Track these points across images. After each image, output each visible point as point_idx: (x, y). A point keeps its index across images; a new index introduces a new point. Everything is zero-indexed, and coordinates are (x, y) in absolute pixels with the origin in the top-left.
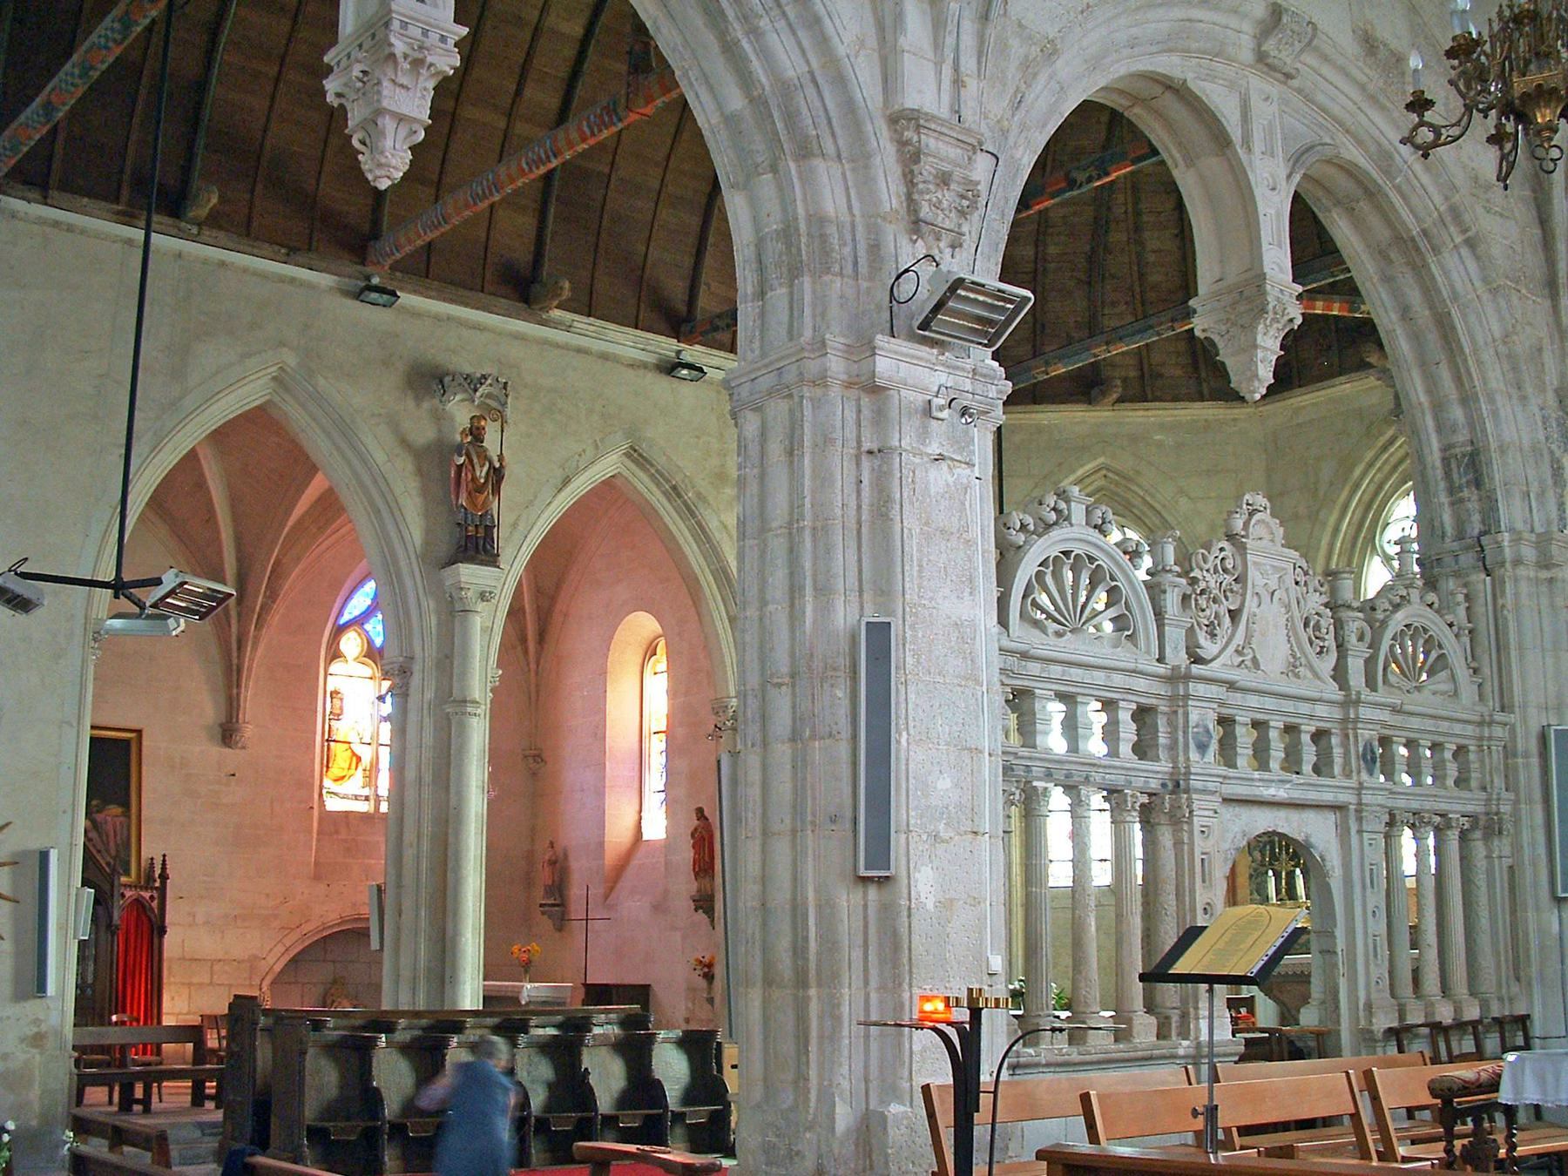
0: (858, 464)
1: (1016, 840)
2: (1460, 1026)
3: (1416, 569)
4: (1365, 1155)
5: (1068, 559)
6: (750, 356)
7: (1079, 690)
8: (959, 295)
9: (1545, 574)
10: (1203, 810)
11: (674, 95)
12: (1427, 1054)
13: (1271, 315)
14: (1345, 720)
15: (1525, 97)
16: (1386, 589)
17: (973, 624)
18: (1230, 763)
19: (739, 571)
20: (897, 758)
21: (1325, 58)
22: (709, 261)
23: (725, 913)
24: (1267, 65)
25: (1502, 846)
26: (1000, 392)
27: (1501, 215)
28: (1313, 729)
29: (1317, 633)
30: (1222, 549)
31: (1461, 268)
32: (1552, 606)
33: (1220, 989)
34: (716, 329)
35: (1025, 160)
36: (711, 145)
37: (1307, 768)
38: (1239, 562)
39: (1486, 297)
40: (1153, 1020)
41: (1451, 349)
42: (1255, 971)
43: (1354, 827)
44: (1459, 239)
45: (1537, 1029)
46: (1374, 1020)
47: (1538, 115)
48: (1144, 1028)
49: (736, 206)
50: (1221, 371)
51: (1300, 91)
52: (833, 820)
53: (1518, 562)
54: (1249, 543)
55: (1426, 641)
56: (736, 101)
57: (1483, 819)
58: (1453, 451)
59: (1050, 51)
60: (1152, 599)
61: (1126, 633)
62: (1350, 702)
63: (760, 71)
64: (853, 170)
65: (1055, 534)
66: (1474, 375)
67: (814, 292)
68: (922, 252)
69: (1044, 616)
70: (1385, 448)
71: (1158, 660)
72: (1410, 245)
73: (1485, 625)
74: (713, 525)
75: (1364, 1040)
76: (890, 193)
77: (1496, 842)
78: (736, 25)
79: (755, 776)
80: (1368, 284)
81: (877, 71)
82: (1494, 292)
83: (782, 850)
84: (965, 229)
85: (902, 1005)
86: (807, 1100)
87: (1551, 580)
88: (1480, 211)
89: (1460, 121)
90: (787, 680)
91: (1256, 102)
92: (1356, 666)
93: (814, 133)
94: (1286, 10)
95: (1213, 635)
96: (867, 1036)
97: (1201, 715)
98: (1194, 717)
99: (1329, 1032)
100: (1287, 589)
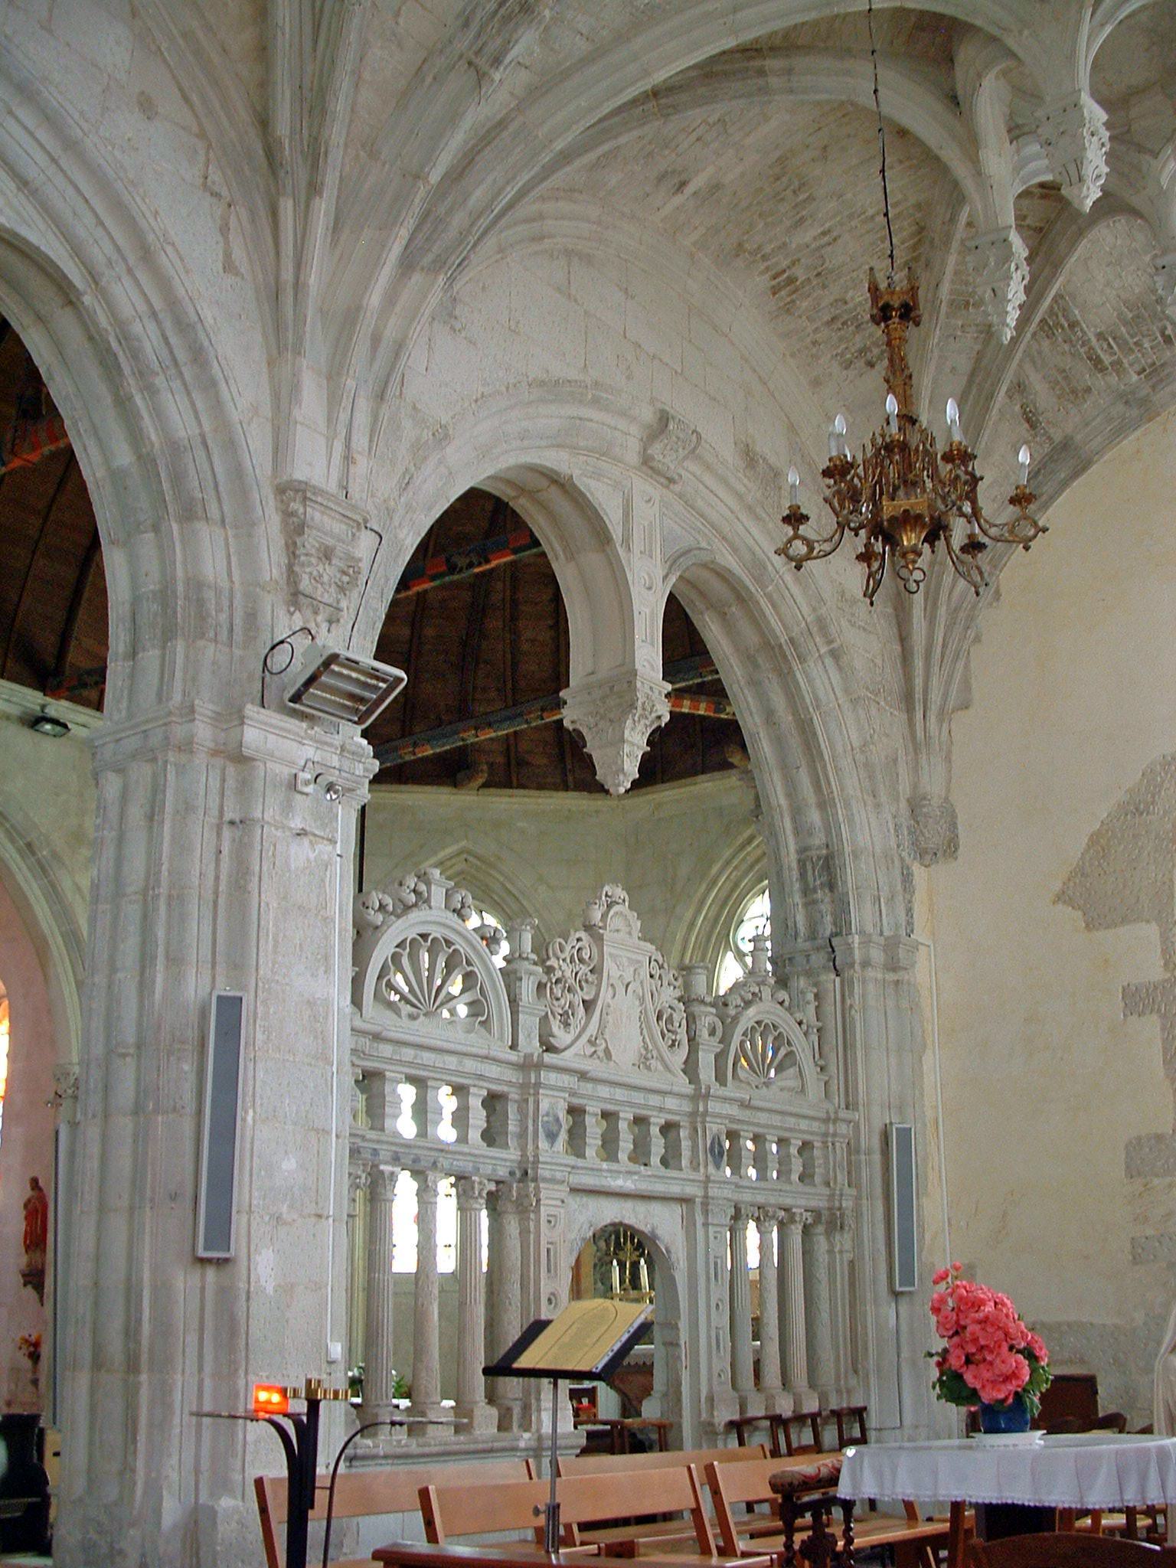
0: (219, 835)
1: (359, 1223)
2: (800, 1419)
3: (769, 967)
4: (706, 1551)
5: (426, 941)
6: (116, 717)
7: (432, 1075)
8: (333, 671)
9: (891, 977)
10: (550, 1199)
11: (62, 444)
12: (768, 1447)
13: (640, 711)
14: (694, 1114)
15: (893, 520)
16: (736, 987)
17: (327, 1002)
18: (581, 1155)
19: (90, 935)
20: (242, 1136)
21: (708, 467)
22: (82, 614)
23: (55, 1289)
24: (651, 468)
25: (844, 1241)
26: (366, 770)
27: (864, 629)
28: (663, 1122)
29: (670, 1027)
30: (579, 940)
31: (824, 677)
32: (898, 1007)
33: (565, 1385)
34: (85, 685)
35: (408, 541)
36: (94, 497)
37: (655, 1160)
38: (595, 950)
39: (846, 706)
40: (494, 1412)
41: (812, 755)
42: (600, 1366)
43: (699, 1219)
44: (823, 650)
45: (873, 1421)
46: (715, 1414)
47: (905, 538)
48: (486, 1418)
49: (115, 563)
50: (588, 764)
51: (681, 496)
52: (174, 1197)
53: (866, 964)
54: (607, 935)
55: (775, 1039)
56: (124, 456)
57: (825, 1213)
58: (808, 853)
59: (442, 436)
60: (508, 987)
61: (480, 1019)
62: (700, 1096)
63: (151, 430)
64: (236, 536)
65: (414, 916)
66: (833, 783)
67: (187, 657)
68: (298, 621)
69: (398, 997)
70: (743, 847)
71: (511, 1048)
72: (776, 650)
73: (833, 1023)
74: (66, 884)
75: (706, 1433)
76: (271, 563)
77: (838, 1237)
78: (132, 381)
79: (95, 1150)
80: (735, 687)
81: (269, 439)
82: (855, 702)
83: (118, 1225)
84: (344, 604)
85: (236, 1395)
86: (133, 1491)
87: (897, 983)
88: (844, 623)
89: (832, 537)
90: (131, 1051)
91: (638, 503)
92: (706, 1060)
93: (200, 496)
94: (673, 418)
95: (567, 1025)
96: (199, 1425)
97: (552, 1104)
98: (544, 1105)
99: (671, 1425)
100: (641, 982)
